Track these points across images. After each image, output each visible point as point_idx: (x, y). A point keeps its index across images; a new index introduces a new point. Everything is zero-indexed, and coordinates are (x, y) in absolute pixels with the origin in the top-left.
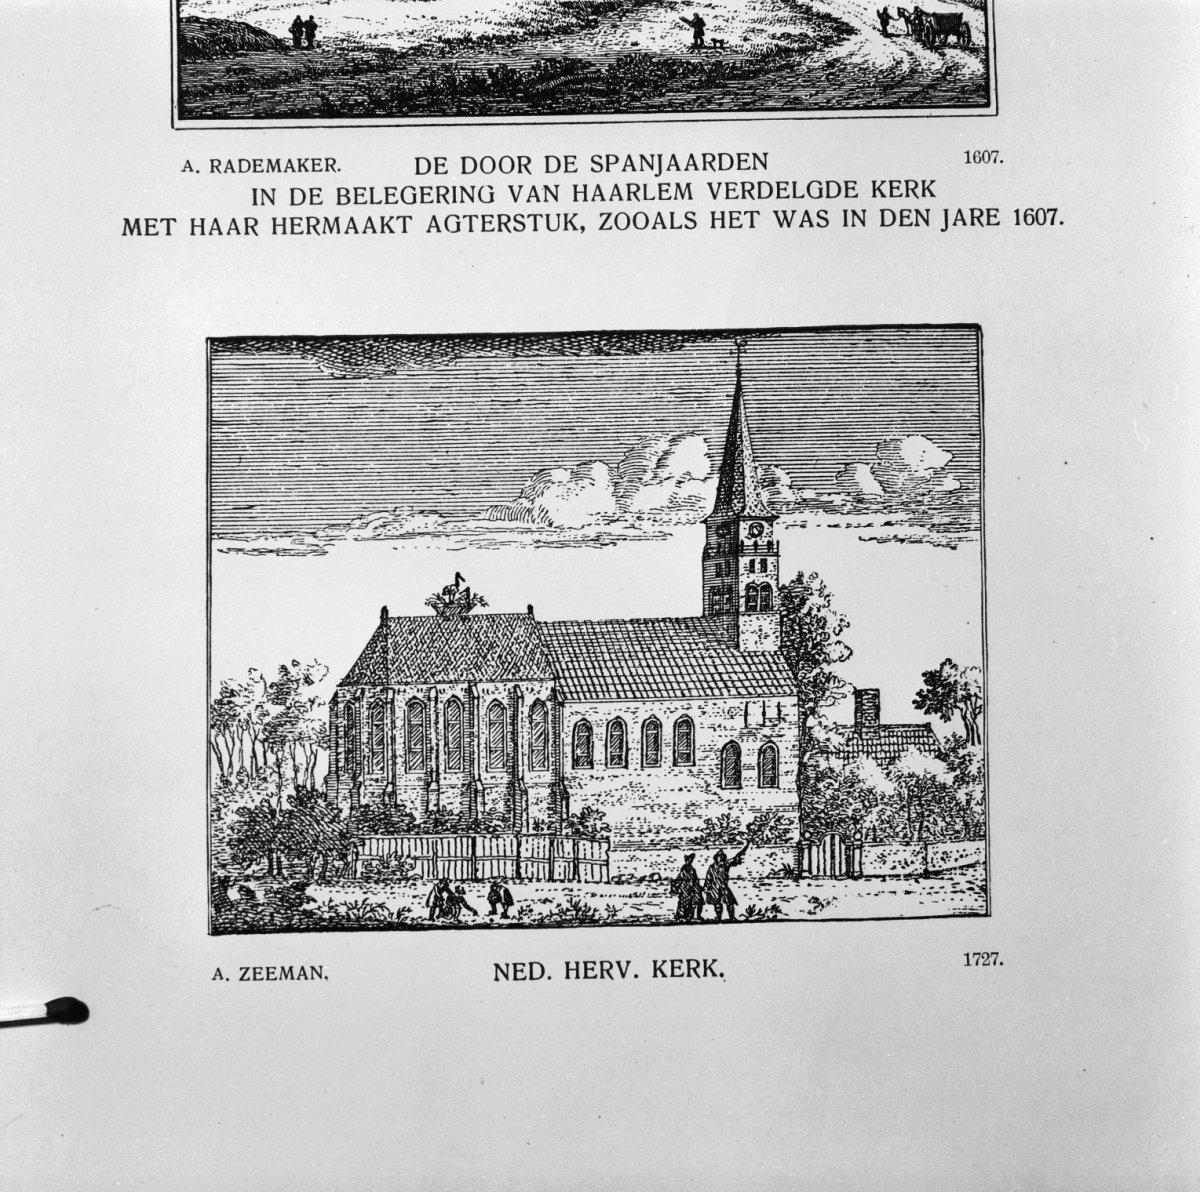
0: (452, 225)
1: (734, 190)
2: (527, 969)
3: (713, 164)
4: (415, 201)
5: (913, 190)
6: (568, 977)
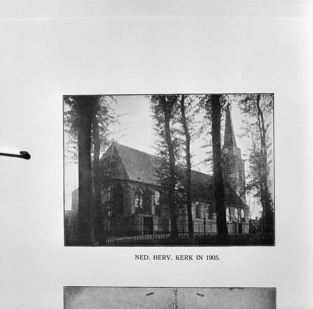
1: (183, 257)
2: (144, 257)
3: (187, 258)
5: (164, 258)
6: (154, 259)
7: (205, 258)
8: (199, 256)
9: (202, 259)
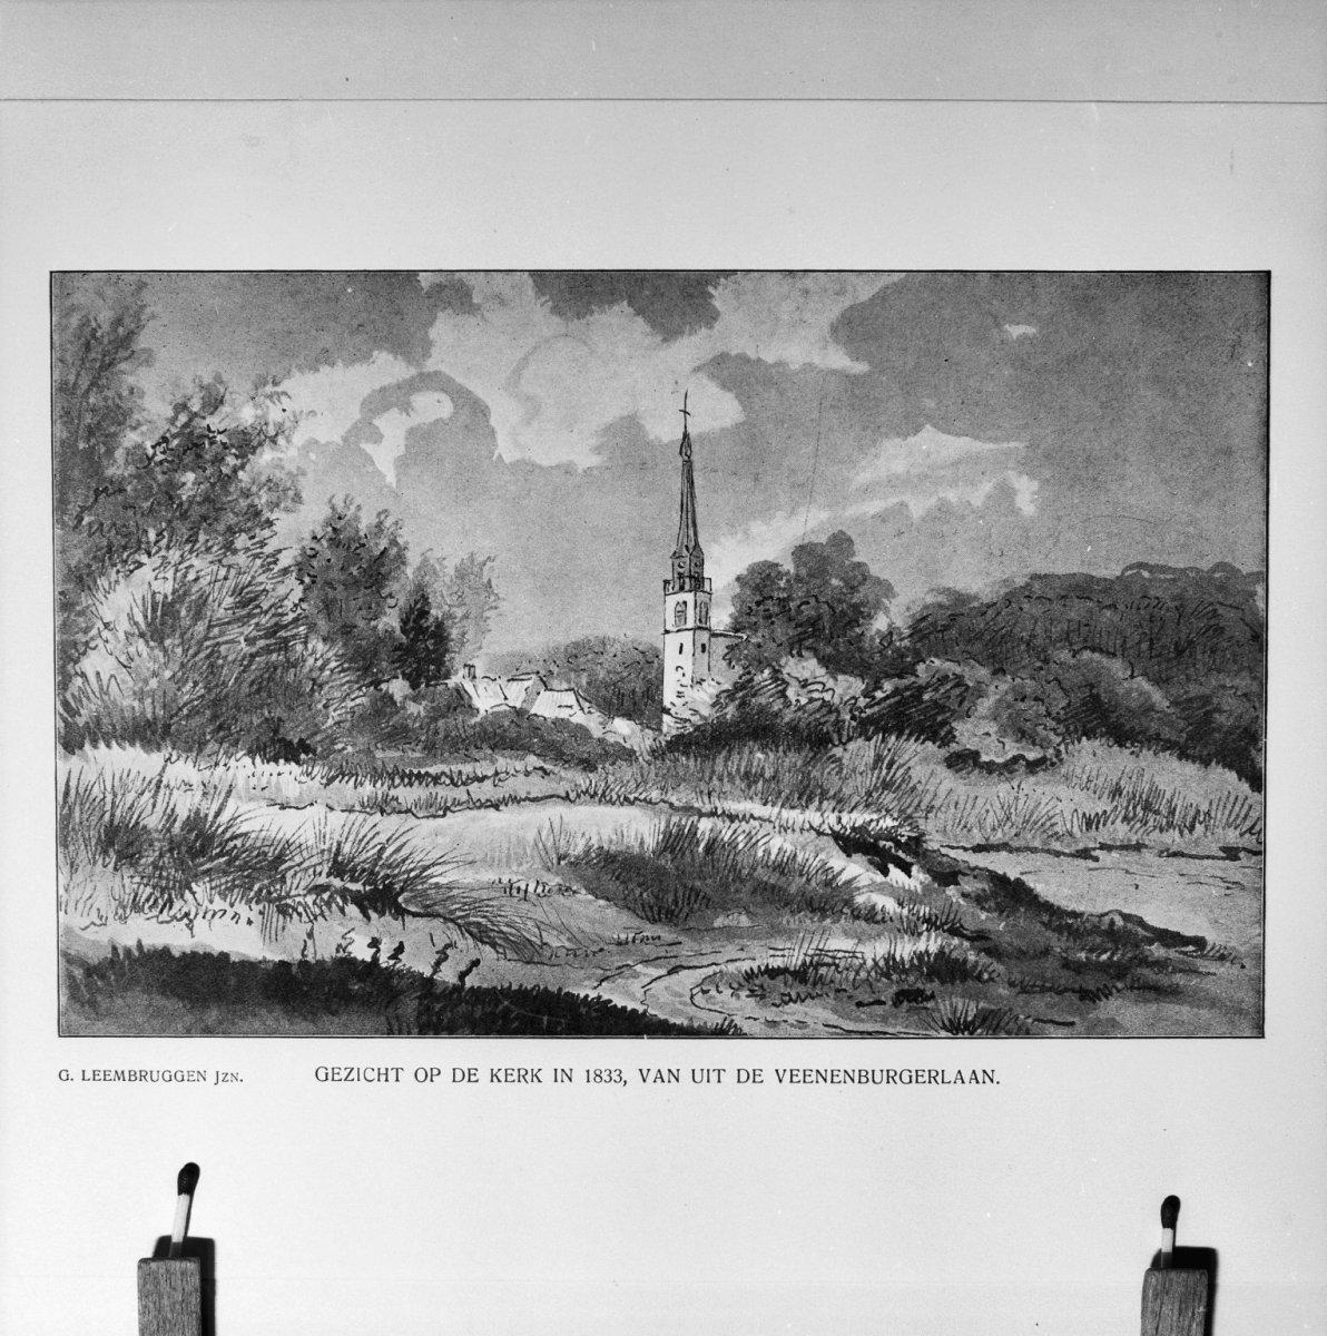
0: (179, 1077)
4: (911, 1082)
7: (579, 1076)
8: (563, 1070)
9: (677, 1080)
